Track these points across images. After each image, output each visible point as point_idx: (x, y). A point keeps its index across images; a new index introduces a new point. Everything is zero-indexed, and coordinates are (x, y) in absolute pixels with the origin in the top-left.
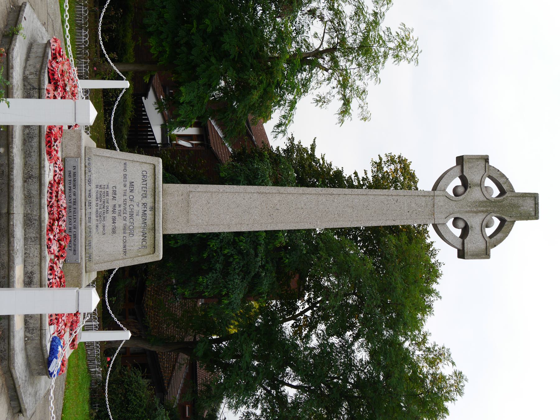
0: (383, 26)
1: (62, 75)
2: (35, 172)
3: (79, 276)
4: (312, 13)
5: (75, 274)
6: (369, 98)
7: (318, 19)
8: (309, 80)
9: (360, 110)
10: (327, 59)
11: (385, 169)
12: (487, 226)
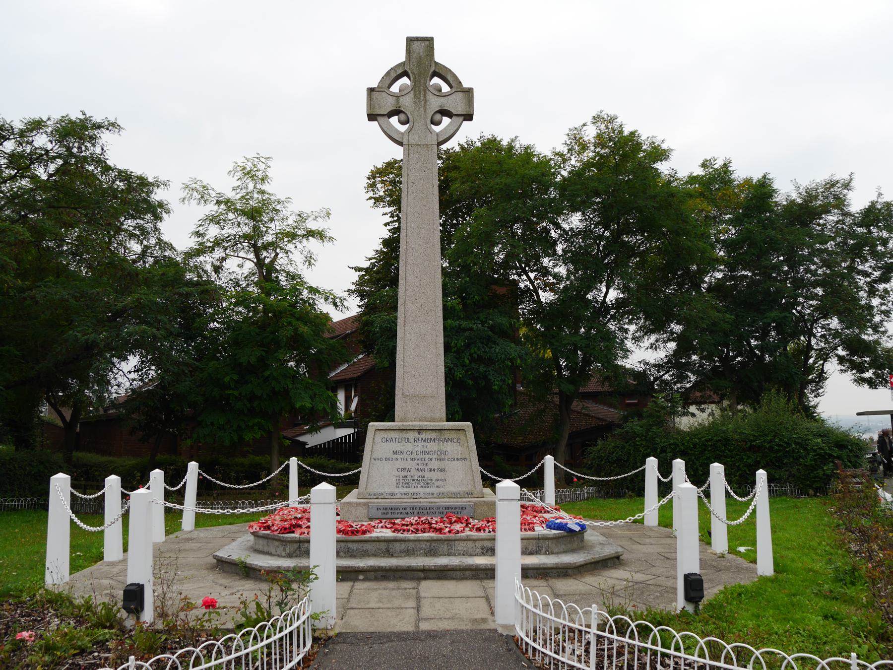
0: (230, 195)
1: (286, 521)
2: (383, 546)
3: (486, 503)
4: (217, 269)
5: (485, 508)
6: (307, 210)
7: (224, 264)
8: (288, 273)
9: (319, 219)
10: (265, 254)
11: (382, 193)
12: (440, 90)
